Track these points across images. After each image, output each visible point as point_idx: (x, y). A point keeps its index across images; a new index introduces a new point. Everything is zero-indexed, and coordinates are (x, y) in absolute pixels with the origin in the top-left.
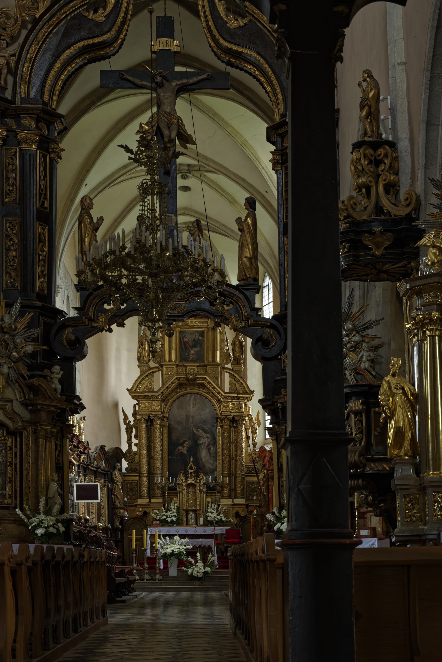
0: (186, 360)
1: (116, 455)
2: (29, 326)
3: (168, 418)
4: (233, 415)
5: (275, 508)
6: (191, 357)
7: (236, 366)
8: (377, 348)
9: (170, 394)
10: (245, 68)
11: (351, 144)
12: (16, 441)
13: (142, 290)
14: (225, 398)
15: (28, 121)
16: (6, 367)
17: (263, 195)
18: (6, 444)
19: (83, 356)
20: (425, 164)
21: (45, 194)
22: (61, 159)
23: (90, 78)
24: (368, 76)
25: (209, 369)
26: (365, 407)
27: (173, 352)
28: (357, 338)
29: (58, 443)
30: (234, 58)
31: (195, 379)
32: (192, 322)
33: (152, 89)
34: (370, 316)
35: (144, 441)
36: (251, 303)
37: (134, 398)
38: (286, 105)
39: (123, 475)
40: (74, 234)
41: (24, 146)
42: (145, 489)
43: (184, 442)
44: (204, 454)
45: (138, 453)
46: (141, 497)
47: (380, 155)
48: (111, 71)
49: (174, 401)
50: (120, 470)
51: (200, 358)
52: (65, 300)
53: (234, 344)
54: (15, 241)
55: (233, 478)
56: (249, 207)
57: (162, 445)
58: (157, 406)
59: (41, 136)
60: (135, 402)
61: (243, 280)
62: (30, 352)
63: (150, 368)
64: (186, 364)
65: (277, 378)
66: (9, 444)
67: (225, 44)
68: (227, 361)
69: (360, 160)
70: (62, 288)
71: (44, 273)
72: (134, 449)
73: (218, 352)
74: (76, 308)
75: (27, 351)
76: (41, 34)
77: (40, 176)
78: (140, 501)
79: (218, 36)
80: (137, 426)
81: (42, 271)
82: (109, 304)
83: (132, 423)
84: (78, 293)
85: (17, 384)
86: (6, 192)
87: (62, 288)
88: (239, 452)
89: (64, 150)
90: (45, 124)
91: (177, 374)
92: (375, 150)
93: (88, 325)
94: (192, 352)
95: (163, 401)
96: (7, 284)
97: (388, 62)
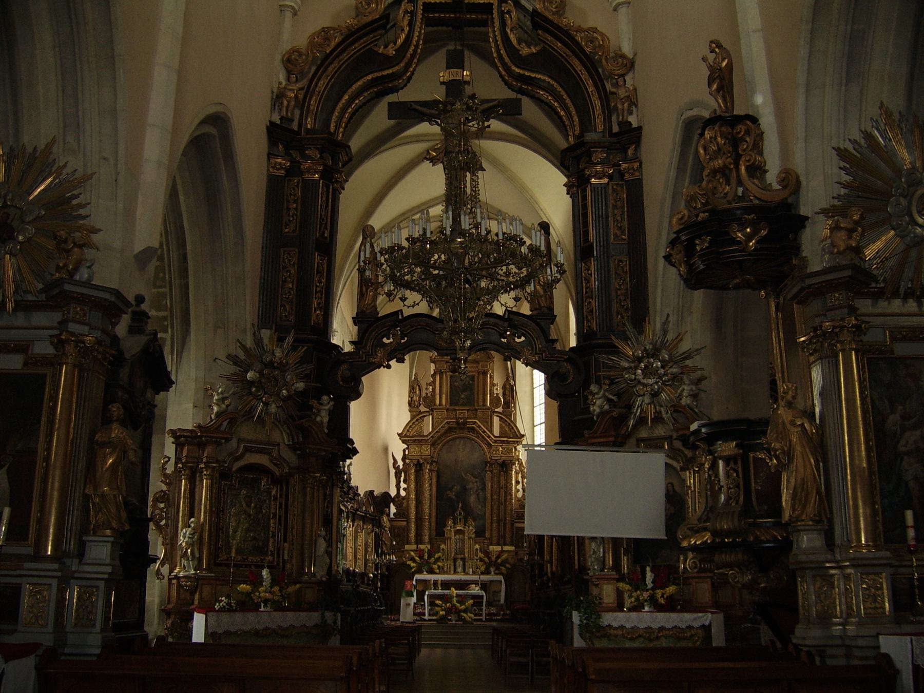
0: (456, 404)
1: (385, 499)
3: (437, 462)
4: (503, 459)
5: (856, 301)
6: (462, 401)
8: (700, 380)
9: (439, 438)
10: (537, 96)
12: (281, 490)
13: (261, 511)
14: (496, 442)
15: (313, 152)
16: (274, 405)
18: (270, 493)
19: (358, 395)
20: (806, 136)
23: (378, 119)
24: (717, 46)
25: (479, 413)
26: (741, 451)
27: (444, 396)
28: (675, 370)
31: (465, 423)
33: (333, 485)
34: (685, 346)
35: (413, 486)
36: (545, 333)
37: (404, 442)
39: (391, 520)
40: (352, 282)
41: (307, 176)
42: (412, 534)
43: (452, 487)
44: (472, 499)
45: (407, 498)
46: (408, 543)
47: (739, 133)
48: (399, 102)
49: (443, 446)
50: (388, 515)
51: (470, 402)
52: (342, 333)
53: (504, 387)
54: (292, 272)
55: (502, 524)
57: (431, 490)
58: (426, 450)
59: (325, 165)
60: (406, 446)
61: (536, 309)
63: (420, 413)
65: (576, 418)
66: (274, 492)
67: (517, 70)
69: (715, 138)
70: (872, 119)
72: (403, 493)
73: (53, 518)
74: (351, 342)
76: (330, 69)
78: (407, 547)
79: (510, 63)
80: (406, 469)
81: (319, 304)
82: (388, 338)
83: (401, 467)
84: (699, 296)
88: (509, 498)
92: (733, 127)
95: (433, 445)
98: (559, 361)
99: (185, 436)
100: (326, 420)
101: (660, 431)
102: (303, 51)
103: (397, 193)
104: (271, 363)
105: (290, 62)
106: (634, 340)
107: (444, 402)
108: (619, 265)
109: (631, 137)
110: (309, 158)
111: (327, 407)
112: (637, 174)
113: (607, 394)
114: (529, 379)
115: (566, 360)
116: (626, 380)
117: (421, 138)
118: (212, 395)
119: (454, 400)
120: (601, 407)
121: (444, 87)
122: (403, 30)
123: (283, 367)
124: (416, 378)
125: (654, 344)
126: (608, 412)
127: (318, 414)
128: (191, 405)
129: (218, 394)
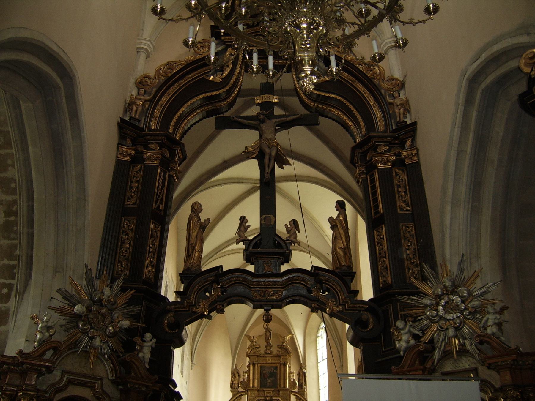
2: (129, 303)
6: (268, 384)
7: (301, 390)
16: (98, 340)
17: (325, 257)
19: (181, 343)
21: (162, 200)
22: (286, 225)
27: (256, 381)
30: (320, 104)
32: (269, 360)
41: (148, 162)
52: (170, 287)
53: (299, 374)
54: (130, 235)
56: (339, 208)
59: (163, 156)
62: (125, 327)
63: (239, 392)
64: (265, 389)
68: (294, 387)
71: (153, 264)
75: (123, 325)
77: (158, 186)
81: (151, 262)
85: (110, 361)
86: (128, 197)
87: (243, 219)
90: (168, 150)
91: (258, 397)
93: (189, 310)
94: (269, 381)
96: (117, 272)
97: (33, 242)
98: (360, 311)
99: (7, 364)
100: (148, 356)
101: (466, 363)
102: (152, 76)
103: (221, 212)
104: (100, 300)
105: (140, 84)
106: (432, 279)
107: (256, 385)
108: (406, 230)
109: (405, 133)
110: (151, 149)
111: (150, 344)
112: (416, 158)
113: (412, 329)
114: (315, 370)
115: (366, 310)
116: (428, 317)
117: (241, 181)
118: (37, 324)
119: (263, 384)
120: (408, 342)
121: (259, 107)
122: (228, 66)
123: (112, 307)
124: (236, 368)
125: (453, 281)
126: (414, 347)
127: (141, 350)
128: (24, 339)
129: (43, 322)
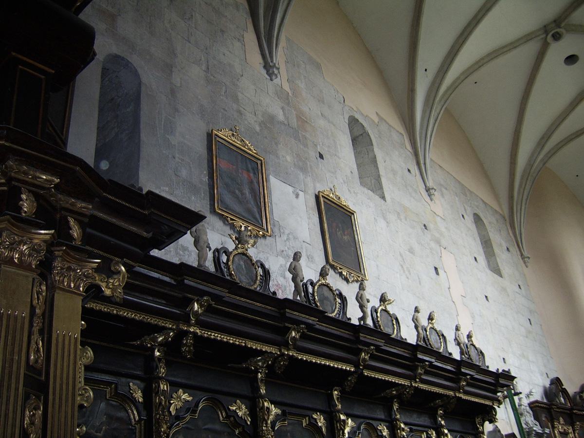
11: (160, 252)
29: (92, 382)
38: (27, 356)
84: (272, 290)
89: (323, 159)
